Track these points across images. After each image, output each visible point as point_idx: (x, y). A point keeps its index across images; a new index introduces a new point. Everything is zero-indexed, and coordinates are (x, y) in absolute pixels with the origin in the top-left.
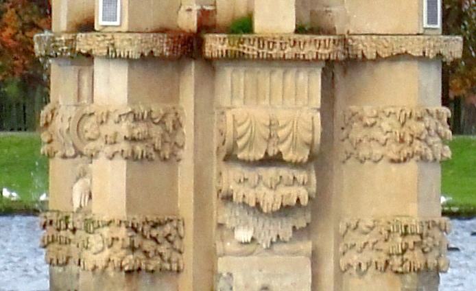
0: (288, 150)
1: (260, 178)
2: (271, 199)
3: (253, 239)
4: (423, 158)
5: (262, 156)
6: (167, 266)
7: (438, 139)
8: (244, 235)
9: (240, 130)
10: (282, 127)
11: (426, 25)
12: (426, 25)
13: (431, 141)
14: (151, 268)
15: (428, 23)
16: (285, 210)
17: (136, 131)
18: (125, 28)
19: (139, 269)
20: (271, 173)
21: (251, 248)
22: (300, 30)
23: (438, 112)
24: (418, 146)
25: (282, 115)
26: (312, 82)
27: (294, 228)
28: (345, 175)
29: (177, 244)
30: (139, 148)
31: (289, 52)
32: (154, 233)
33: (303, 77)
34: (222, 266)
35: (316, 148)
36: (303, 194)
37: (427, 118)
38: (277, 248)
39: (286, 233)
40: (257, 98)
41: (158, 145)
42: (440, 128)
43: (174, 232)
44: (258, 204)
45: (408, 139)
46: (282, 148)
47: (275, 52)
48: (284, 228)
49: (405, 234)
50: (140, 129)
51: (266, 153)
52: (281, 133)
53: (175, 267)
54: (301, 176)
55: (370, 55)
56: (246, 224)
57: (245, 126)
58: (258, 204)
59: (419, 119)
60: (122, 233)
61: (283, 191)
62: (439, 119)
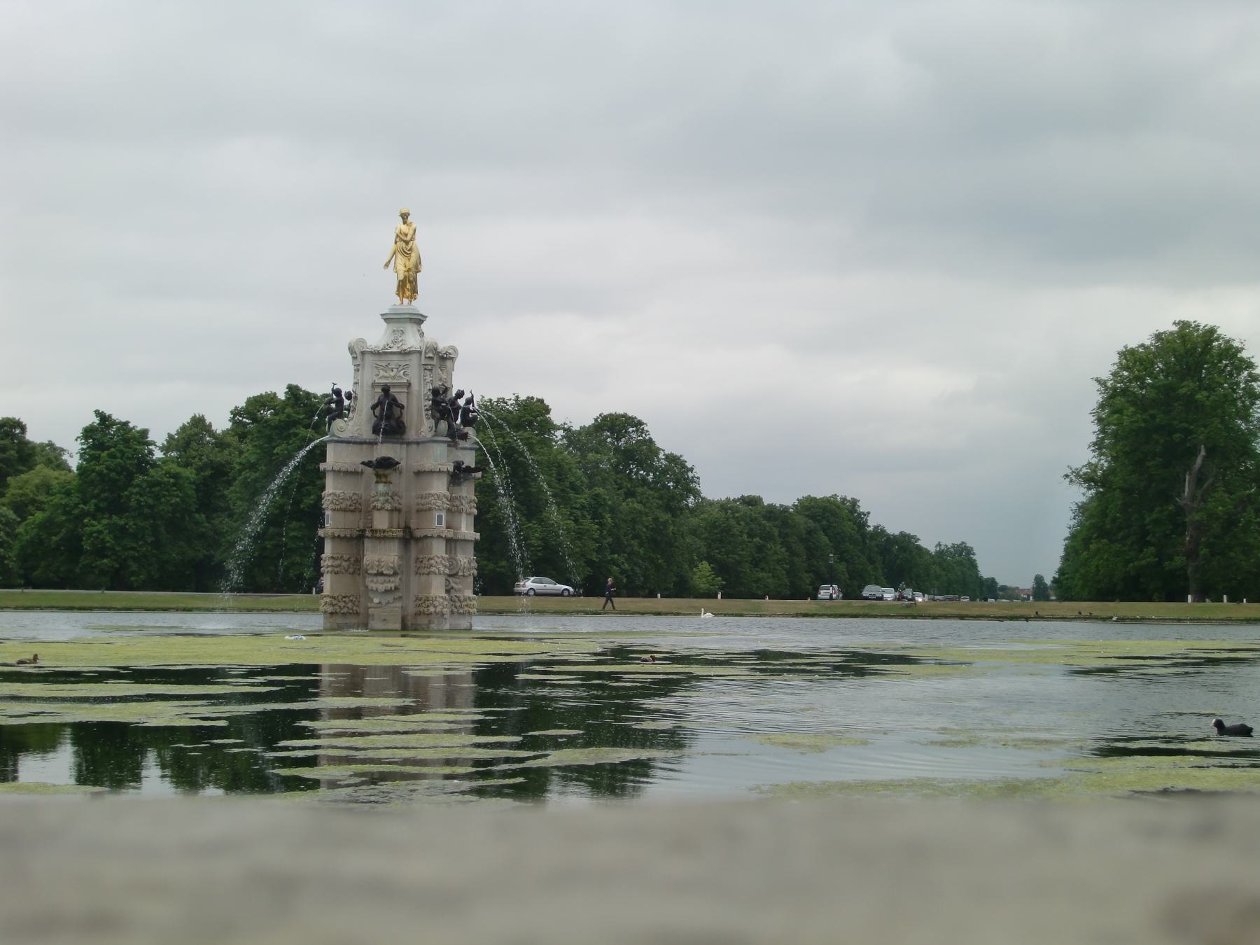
2: (381, 588)
5: (376, 572)
6: (351, 611)
8: (376, 600)
16: (387, 591)
20: (381, 579)
23: (442, 557)
25: (384, 558)
27: (394, 598)
29: (356, 603)
30: (336, 570)
42: (443, 562)
50: (338, 562)
51: (378, 571)
52: (382, 564)
53: (355, 612)
56: (377, 597)
58: (377, 590)
61: (386, 585)
62: (443, 559)
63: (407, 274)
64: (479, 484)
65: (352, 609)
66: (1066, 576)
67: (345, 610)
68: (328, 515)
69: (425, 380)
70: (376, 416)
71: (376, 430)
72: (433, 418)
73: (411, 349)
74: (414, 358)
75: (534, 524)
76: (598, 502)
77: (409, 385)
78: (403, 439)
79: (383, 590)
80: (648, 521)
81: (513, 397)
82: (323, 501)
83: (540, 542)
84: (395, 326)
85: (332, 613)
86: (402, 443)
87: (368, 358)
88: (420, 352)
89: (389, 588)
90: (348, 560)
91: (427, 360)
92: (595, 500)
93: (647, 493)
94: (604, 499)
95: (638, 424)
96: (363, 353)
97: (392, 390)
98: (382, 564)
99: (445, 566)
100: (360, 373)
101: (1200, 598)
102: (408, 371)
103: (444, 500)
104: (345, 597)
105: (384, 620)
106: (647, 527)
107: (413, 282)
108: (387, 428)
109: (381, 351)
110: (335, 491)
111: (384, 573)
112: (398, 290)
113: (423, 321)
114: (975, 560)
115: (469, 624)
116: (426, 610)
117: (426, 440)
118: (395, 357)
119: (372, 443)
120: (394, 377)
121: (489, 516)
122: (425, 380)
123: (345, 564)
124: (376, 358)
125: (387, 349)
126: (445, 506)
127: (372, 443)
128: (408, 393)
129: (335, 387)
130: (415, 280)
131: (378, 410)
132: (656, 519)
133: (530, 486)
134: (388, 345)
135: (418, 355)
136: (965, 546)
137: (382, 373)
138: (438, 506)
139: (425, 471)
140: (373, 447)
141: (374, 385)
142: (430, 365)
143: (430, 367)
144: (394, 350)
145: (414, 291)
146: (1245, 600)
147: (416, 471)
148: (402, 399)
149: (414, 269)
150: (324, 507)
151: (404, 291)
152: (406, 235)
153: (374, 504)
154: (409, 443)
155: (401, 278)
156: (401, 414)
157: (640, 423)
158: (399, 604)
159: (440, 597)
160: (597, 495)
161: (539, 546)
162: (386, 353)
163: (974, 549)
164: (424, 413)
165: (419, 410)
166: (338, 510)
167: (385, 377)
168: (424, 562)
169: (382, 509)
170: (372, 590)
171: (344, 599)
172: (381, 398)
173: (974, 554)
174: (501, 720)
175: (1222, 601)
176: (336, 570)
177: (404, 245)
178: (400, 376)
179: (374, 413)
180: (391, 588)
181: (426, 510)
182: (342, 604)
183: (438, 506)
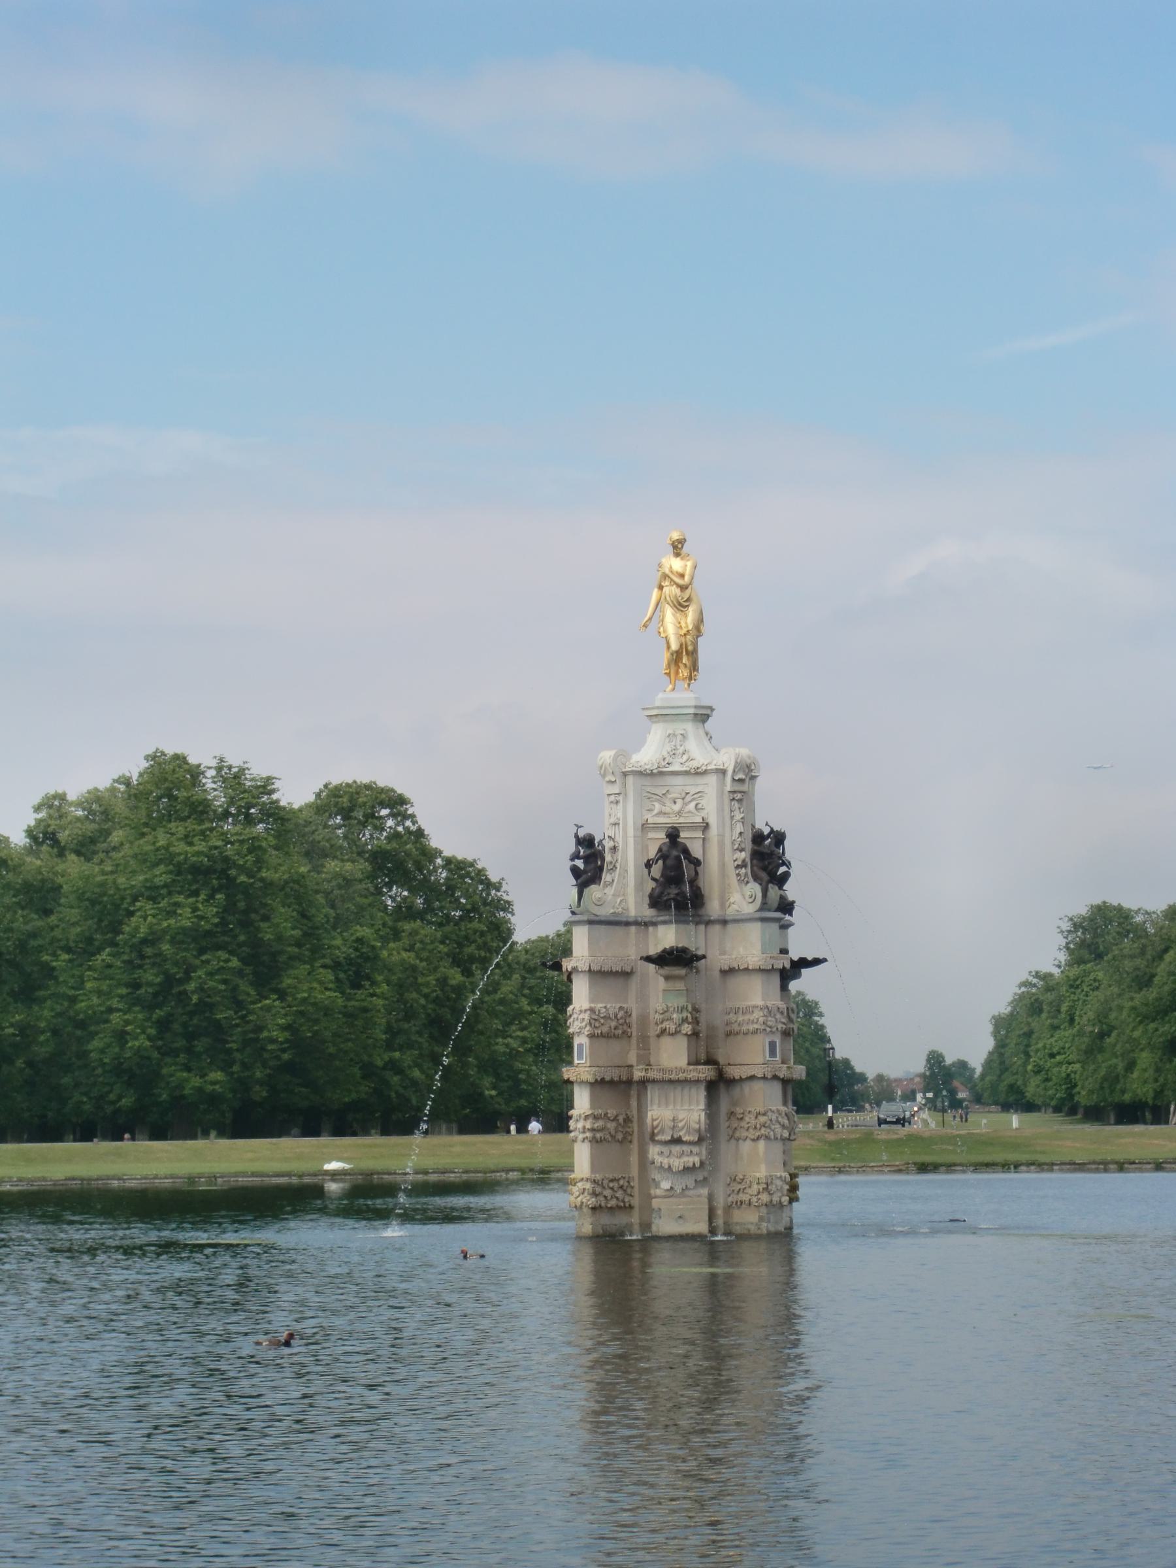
0: (685, 1135)
1: (671, 1152)
2: (677, 1164)
3: (671, 1188)
4: (767, 1138)
5: (669, 1138)
6: (622, 1204)
7: (778, 1126)
8: (665, 1185)
9: (655, 1123)
10: (681, 1121)
11: (768, 1058)
12: (768, 1058)
13: (773, 1127)
14: (609, 1206)
15: (770, 1056)
16: (687, 1170)
17: (596, 1125)
18: (588, 1064)
19: (750, 1204)
20: (677, 1149)
21: (671, 1193)
22: (689, 1064)
23: (778, 1111)
24: (763, 1131)
25: (681, 1115)
26: (701, 1094)
27: (696, 1181)
28: (726, 1148)
29: (629, 1191)
30: (598, 1135)
31: (681, 1076)
32: (611, 1185)
33: (694, 1091)
34: (655, 1203)
35: (703, 1133)
36: (697, 1160)
37: (770, 1114)
38: (687, 1192)
39: (691, 1184)
40: (667, 1104)
41: (613, 1132)
42: (780, 1119)
43: (626, 1184)
44: (670, 1167)
45: (758, 1126)
46: (681, 1133)
47: (673, 1077)
48: (689, 1181)
49: (758, 1183)
50: (599, 1124)
51: (672, 1136)
52: (680, 1125)
53: (627, 1205)
54: (695, 1149)
55: (737, 1078)
56: (667, 1179)
57: (683, 1123)
58: (670, 1167)
59: (764, 1114)
60: (588, 1186)
61: (685, 1159)
62: (780, 1114)
63: (683, 639)
65: (623, 1201)
66: (1058, 1058)
67: (613, 1203)
68: (580, 1046)
69: (732, 818)
70: (654, 879)
71: (656, 902)
72: (755, 880)
73: (709, 768)
74: (712, 779)
75: (274, 1001)
76: (362, 954)
77: (706, 827)
78: (699, 916)
79: (681, 1168)
80: (427, 984)
81: (214, 763)
82: (571, 1020)
83: (287, 1034)
84: (671, 728)
85: (594, 1209)
86: (697, 923)
87: (630, 779)
88: (723, 772)
89: (691, 1165)
90: (615, 1119)
91: (735, 784)
92: (356, 949)
93: (423, 932)
94: (373, 947)
95: (397, 803)
96: (625, 774)
97: (682, 835)
99: (783, 1127)
100: (621, 805)
102: (703, 802)
103: (778, 1016)
104: (612, 1181)
105: (680, 1217)
106: (426, 996)
107: (693, 654)
108: (679, 898)
109: (655, 771)
110: (593, 1005)
111: (684, 1139)
112: (669, 666)
113: (708, 716)
114: (823, 1027)
115: (788, 1219)
116: (754, 1199)
117: (743, 917)
118: (679, 780)
119: (644, 924)
120: (679, 813)
121: (192, 986)
122: (732, 818)
123: (611, 1126)
124: (647, 781)
125: (664, 767)
126: (780, 1026)
127: (644, 924)
129: (581, 834)
130: (695, 651)
131: (657, 870)
132: (443, 982)
133: (258, 929)
134: (664, 759)
135: (721, 775)
136: (803, 1000)
137: (657, 807)
138: (770, 1027)
139: (747, 969)
140: (647, 931)
141: (645, 827)
142: (740, 792)
143: (739, 796)
144: (676, 767)
145: (694, 667)
147: (726, 968)
148: (696, 850)
149: (693, 633)
150: (571, 1030)
151: (679, 667)
152: (682, 576)
153: (663, 1026)
154: (708, 923)
155: (674, 646)
156: (697, 873)
157: (402, 801)
158: (704, 1191)
159: (777, 1178)
160: (360, 940)
161: (287, 1041)
162: (661, 773)
163: (820, 1004)
164: (732, 872)
165: (723, 866)
167: (665, 814)
168: (747, 1119)
169: (677, 1032)
170: (661, 1167)
171: (611, 1185)
172: (665, 849)
173: (821, 1015)
176: (598, 1135)
177: (678, 591)
179: (649, 872)
180: (694, 1164)
181: (746, 1034)
182: (608, 1193)
183: (770, 1027)
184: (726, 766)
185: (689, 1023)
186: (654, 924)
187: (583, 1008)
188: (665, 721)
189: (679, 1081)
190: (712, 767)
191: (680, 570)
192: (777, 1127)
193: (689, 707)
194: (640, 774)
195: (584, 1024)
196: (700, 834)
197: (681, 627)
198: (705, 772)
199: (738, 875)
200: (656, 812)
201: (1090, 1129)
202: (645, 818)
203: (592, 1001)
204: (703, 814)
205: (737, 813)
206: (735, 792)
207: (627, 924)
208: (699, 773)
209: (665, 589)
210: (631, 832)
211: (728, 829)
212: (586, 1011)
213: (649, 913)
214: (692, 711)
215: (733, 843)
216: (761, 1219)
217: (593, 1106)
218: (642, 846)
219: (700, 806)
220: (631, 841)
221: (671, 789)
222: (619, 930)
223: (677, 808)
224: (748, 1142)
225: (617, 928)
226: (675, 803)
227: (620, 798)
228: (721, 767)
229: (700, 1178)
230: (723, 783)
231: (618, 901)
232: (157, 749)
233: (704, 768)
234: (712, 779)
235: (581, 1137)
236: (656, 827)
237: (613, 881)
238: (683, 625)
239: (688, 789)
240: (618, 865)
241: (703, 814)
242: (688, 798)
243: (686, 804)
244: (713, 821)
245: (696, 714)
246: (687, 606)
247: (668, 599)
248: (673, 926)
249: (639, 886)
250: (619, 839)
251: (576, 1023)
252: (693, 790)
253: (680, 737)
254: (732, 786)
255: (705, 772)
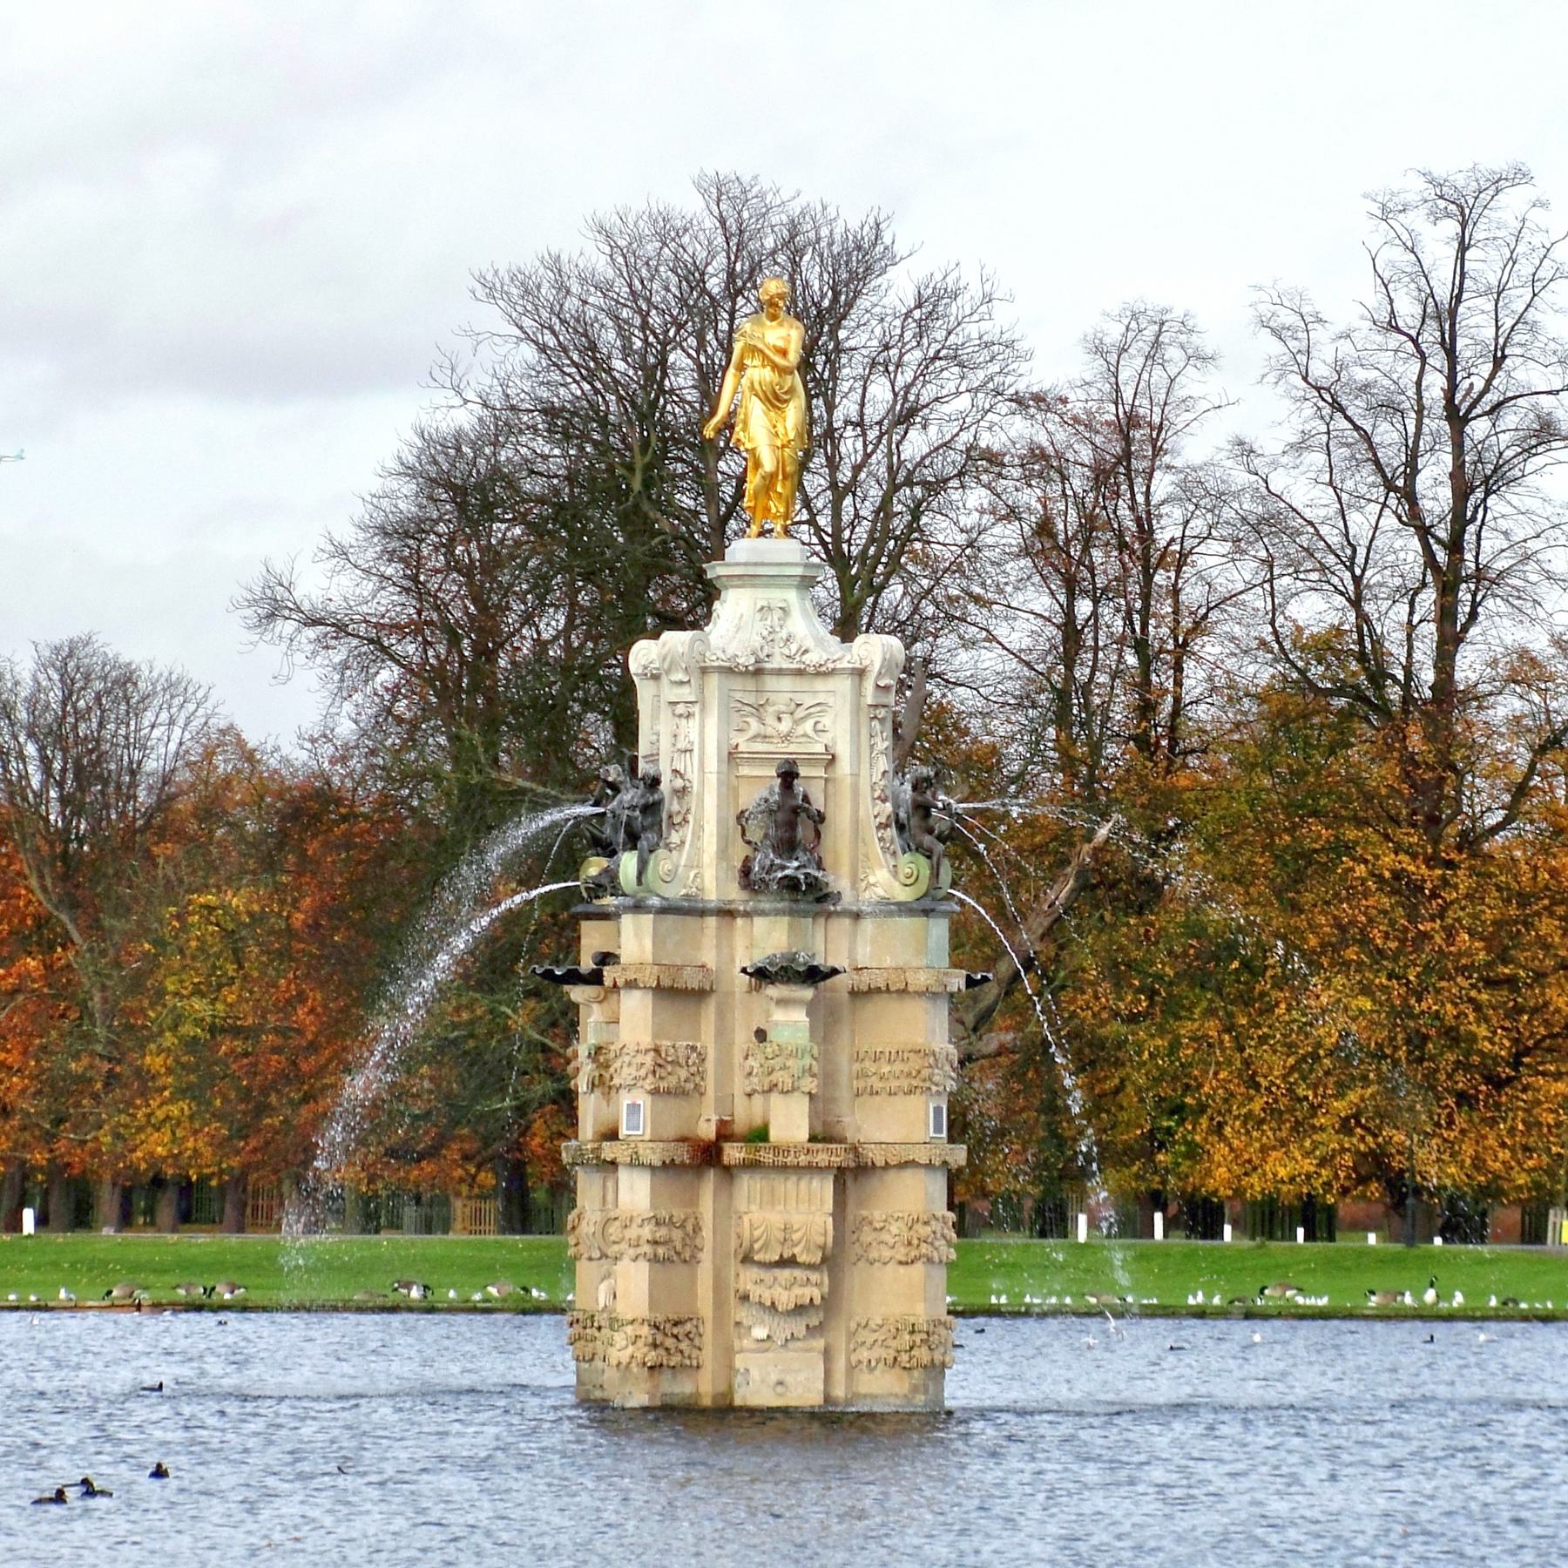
2: (785, 1299)
4: (930, 1260)
5: (777, 1258)
8: (760, 1332)
9: (757, 1233)
13: (937, 1244)
16: (799, 1310)
18: (647, 1137)
20: (785, 1274)
21: (767, 1345)
24: (924, 1248)
25: (797, 1220)
26: (825, 1188)
28: (856, 1277)
30: (661, 1251)
31: (803, 1159)
32: (675, 1331)
33: (816, 1183)
36: (816, 1294)
37: (933, 1223)
38: (791, 1345)
44: (773, 1303)
45: (915, 1242)
46: (796, 1250)
47: (790, 1160)
48: (798, 1326)
49: (912, 1332)
50: (662, 1233)
52: (796, 1237)
54: (815, 1277)
55: (880, 1162)
58: (773, 1303)
60: (645, 1331)
61: (797, 1291)
64: (959, 922)
73: (839, 666)
87: (713, 680)
96: (704, 671)
98: (796, 1237)
101: (125, 1220)
102: (826, 721)
118: (786, 683)
120: (786, 738)
122: (872, 746)
128: (826, 780)
135: (857, 678)
141: (732, 757)
146: (1300, 1232)
165: (856, 821)
166: (668, 1092)
169: (794, 1089)
171: (675, 1331)
174: (1204, 1218)
175: (1150, 1233)
178: (805, 735)
184: (865, 663)
185: (814, 1076)
186: (747, 914)
187: (642, 1047)
188: (753, 586)
189: (797, 1168)
190: (844, 664)
191: (780, 344)
192: (941, 1243)
193: (797, 565)
194: (729, 671)
195: (643, 1072)
196: (821, 772)
197: (777, 435)
198: (832, 673)
199: (881, 839)
200: (751, 733)
201: (623, 934)
202: (734, 742)
203: (655, 1036)
204: (826, 738)
205: (878, 739)
206: (876, 706)
207: (703, 913)
208: (822, 673)
209: (749, 372)
210: (712, 764)
211: (865, 766)
212: (647, 1051)
213: (735, 894)
214: (799, 571)
215: (873, 790)
216: (915, 1389)
217: (653, 1206)
218: (729, 790)
219: (820, 727)
220: (712, 780)
221: (773, 697)
222: (691, 921)
223: (784, 727)
224: (892, 1266)
225: (689, 919)
226: (779, 719)
227: (696, 709)
228: (857, 665)
229: (814, 1322)
230: (859, 693)
231: (692, 875)
232: (231, 727)
233: (831, 666)
234: (844, 685)
235: (632, 1252)
236: (755, 759)
237: (683, 842)
238: (780, 429)
239: (798, 698)
240: (690, 818)
241: (826, 738)
242: (800, 713)
243: (797, 722)
244: (843, 750)
245: (803, 577)
246: (786, 401)
247: (757, 386)
248: (786, 919)
249: (723, 852)
250: (693, 775)
251: (625, 1070)
252: (808, 700)
253: (778, 614)
254: (875, 697)
255: (832, 673)
